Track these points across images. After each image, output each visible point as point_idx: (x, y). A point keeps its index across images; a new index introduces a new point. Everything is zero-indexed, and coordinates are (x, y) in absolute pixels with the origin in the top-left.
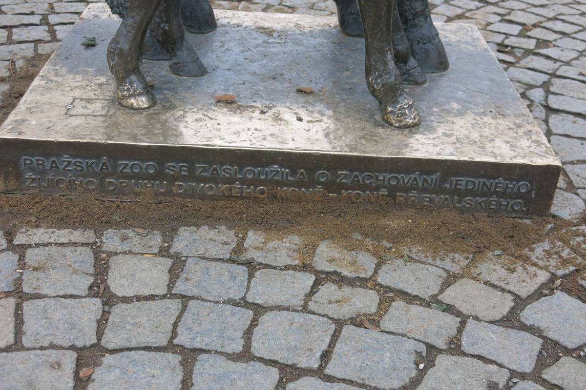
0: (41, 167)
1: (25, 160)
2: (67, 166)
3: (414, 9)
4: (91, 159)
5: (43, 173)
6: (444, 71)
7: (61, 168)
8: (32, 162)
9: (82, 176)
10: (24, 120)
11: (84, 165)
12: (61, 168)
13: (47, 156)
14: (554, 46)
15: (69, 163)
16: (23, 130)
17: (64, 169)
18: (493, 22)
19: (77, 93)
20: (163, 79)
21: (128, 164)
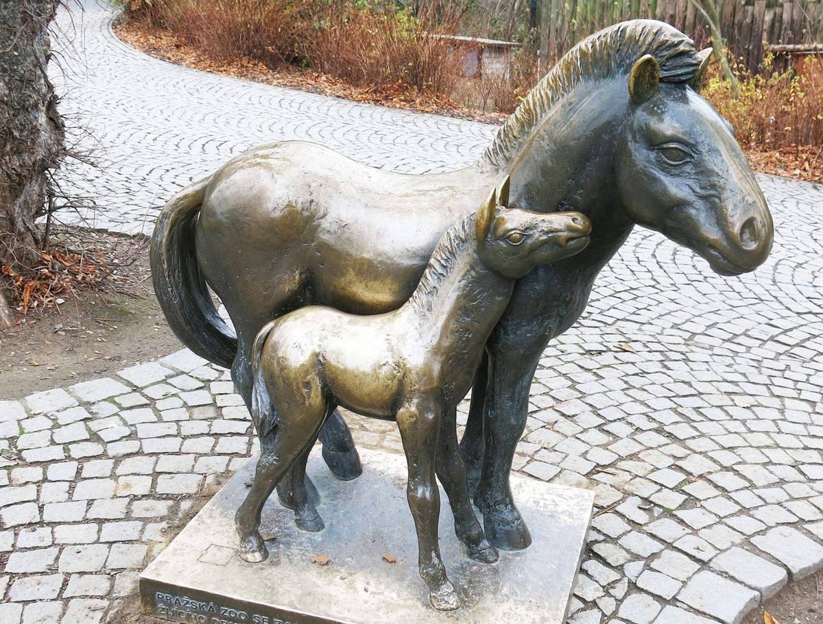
0: (169, 601)
1: (158, 595)
2: (186, 604)
3: (495, 498)
4: (203, 602)
5: (171, 605)
6: (523, 548)
7: (182, 604)
8: (163, 597)
9: (196, 612)
10: (166, 562)
11: (198, 605)
12: (182, 604)
13: (174, 595)
14: (702, 506)
15: (188, 602)
16: (161, 572)
17: (184, 605)
18: (660, 468)
19: (214, 540)
20: (286, 531)
21: (227, 610)
